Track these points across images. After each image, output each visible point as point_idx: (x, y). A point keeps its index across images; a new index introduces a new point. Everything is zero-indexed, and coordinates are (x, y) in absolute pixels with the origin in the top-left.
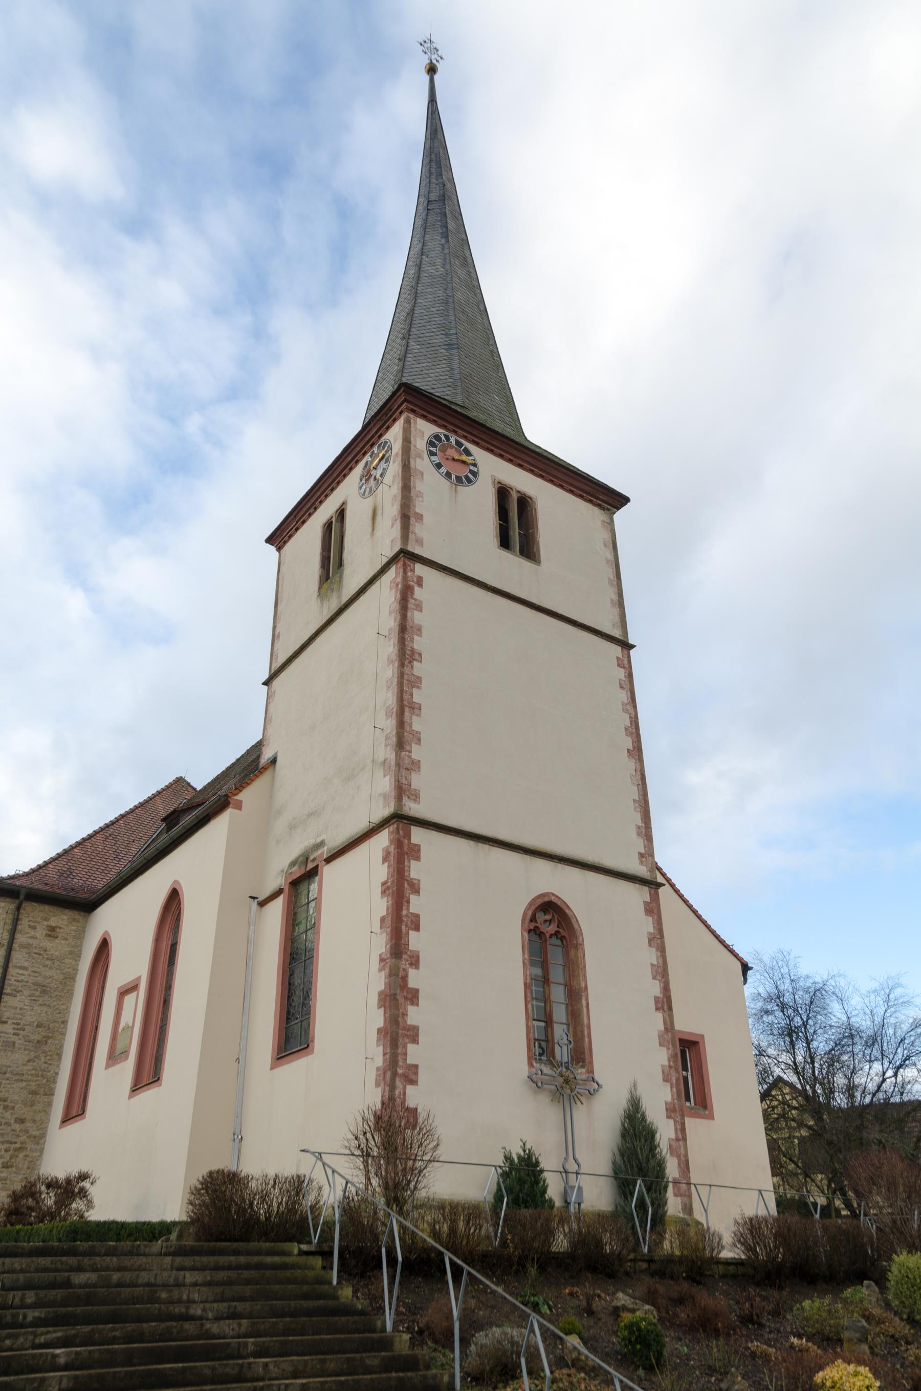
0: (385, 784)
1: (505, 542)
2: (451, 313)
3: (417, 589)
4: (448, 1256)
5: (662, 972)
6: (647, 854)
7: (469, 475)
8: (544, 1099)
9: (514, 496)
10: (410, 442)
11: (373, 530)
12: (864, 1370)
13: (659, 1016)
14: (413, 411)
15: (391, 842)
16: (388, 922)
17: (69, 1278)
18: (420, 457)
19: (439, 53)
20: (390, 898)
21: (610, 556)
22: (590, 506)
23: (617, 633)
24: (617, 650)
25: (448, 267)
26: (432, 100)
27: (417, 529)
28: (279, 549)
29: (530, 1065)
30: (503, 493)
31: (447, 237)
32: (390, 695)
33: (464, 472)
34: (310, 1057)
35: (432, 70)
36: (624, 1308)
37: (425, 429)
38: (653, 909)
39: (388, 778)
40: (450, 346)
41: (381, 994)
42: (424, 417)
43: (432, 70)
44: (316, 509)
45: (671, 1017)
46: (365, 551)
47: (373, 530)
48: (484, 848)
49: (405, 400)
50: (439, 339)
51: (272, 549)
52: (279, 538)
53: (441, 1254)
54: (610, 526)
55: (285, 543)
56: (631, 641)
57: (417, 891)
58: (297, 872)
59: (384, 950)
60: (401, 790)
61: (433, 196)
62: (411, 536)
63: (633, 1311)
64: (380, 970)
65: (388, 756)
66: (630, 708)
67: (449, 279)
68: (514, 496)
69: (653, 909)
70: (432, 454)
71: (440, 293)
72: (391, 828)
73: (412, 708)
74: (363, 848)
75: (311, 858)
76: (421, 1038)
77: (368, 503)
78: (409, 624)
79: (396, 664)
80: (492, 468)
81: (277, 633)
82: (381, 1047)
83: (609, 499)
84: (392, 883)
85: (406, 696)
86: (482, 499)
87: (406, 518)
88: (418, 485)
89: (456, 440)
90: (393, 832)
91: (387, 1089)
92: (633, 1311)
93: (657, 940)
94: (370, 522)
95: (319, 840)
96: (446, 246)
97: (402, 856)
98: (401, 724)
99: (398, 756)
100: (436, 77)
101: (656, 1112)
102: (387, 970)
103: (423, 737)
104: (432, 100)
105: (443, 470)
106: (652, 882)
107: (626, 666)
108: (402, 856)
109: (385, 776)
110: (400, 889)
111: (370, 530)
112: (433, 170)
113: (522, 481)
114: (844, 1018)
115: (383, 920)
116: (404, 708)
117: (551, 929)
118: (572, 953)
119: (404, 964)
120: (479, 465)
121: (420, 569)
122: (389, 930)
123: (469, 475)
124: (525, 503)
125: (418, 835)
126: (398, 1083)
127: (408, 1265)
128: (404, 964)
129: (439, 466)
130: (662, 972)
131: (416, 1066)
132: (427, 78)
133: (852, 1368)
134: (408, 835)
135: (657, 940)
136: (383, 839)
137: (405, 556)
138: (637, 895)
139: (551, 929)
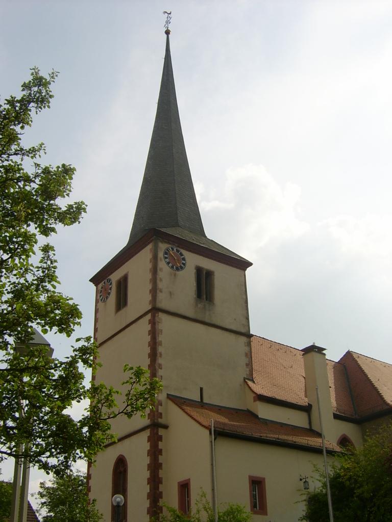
7: (182, 265)
17: (70, 167)
35: (167, 32)
39: (150, 336)
43: (167, 32)
46: (139, 299)
70: (166, 258)
74: (141, 320)
80: (193, 260)
83: (243, 264)
86: (188, 278)
87: (154, 291)
88: (161, 275)
100: (170, 36)
105: (170, 265)
108: (154, 317)
109: (149, 335)
110: (154, 333)
113: (207, 264)
114: (305, 502)
120: (186, 260)
123: (182, 265)
129: (168, 263)
132: (166, 36)
136: (149, 316)
137: (155, 310)
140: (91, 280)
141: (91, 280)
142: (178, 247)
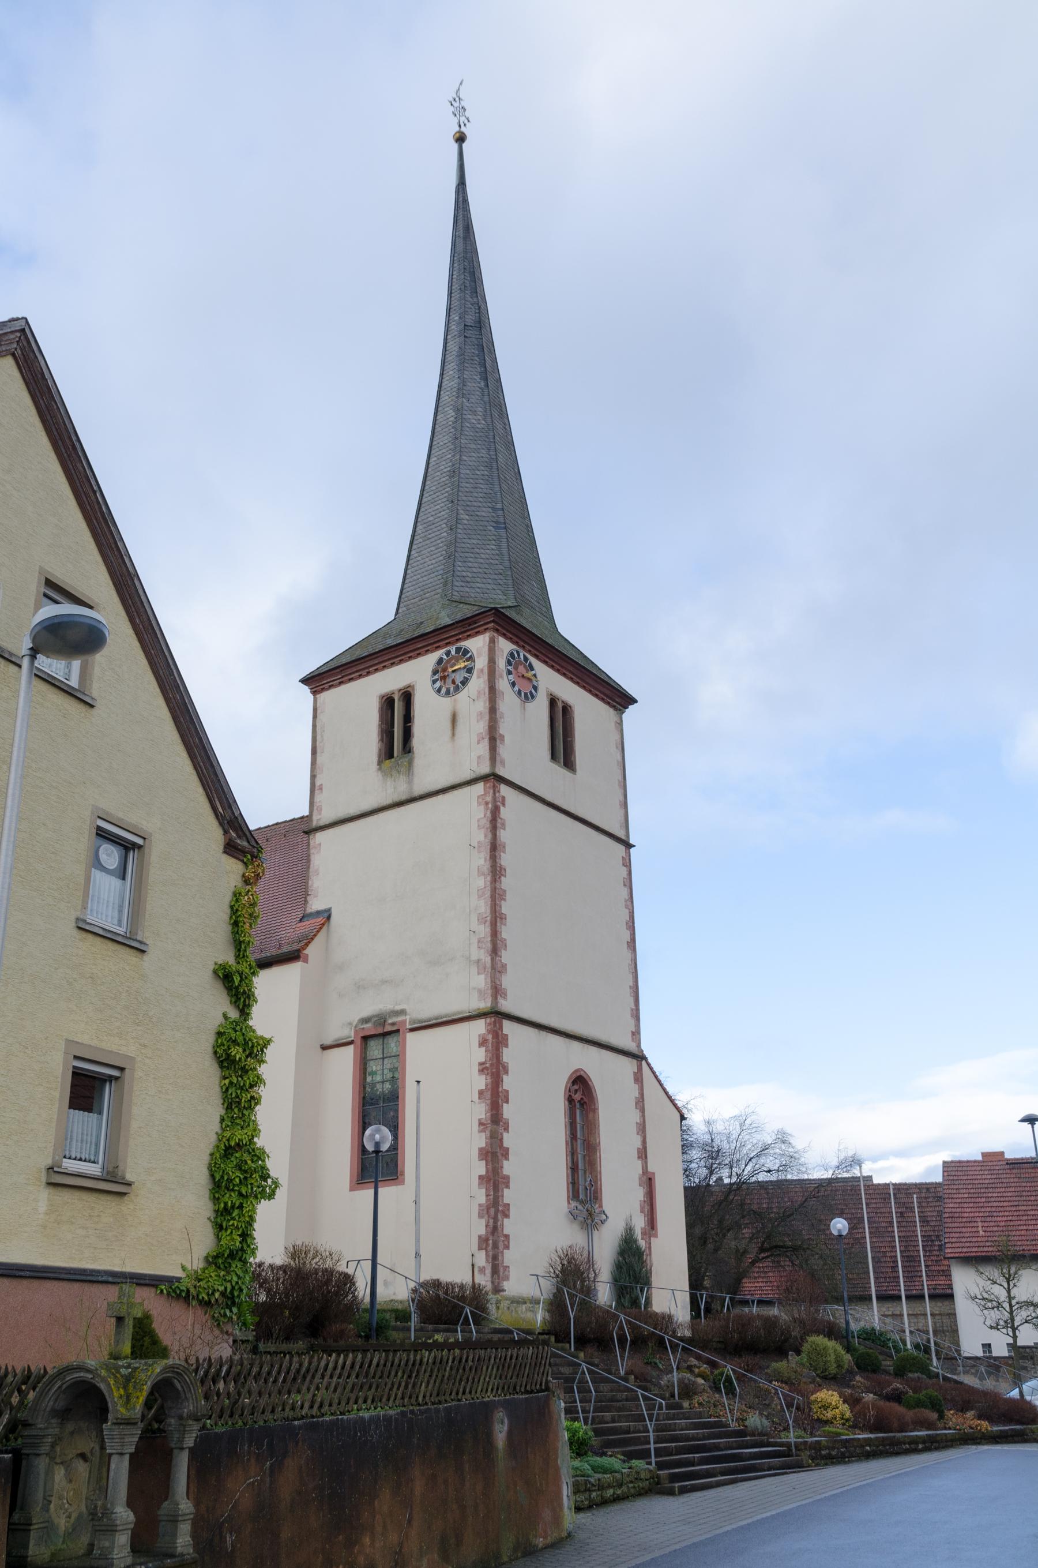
0: (481, 981)
1: (554, 757)
2: (496, 483)
3: (502, 808)
4: (666, 1337)
5: (642, 1129)
6: (636, 1034)
8: (576, 1227)
9: (560, 705)
10: (495, 663)
11: (453, 735)
12: (835, 1393)
13: (640, 1162)
14: (497, 631)
15: (489, 1031)
16: (488, 1095)
18: (501, 676)
19: (467, 113)
20: (489, 1077)
21: (620, 758)
22: (607, 707)
23: (621, 834)
24: (622, 848)
25: (489, 419)
26: (461, 184)
27: (503, 751)
28: (314, 693)
29: (569, 1203)
30: (553, 701)
31: (486, 379)
32: (482, 903)
33: (528, 688)
34: (399, 1187)
35: (461, 139)
36: (695, 1366)
37: (505, 646)
38: (638, 1078)
40: (497, 525)
41: (481, 1150)
42: (504, 636)
43: (461, 139)
44: (368, 673)
45: (646, 1163)
47: (453, 735)
48: (544, 1034)
49: (493, 621)
50: (485, 512)
51: (306, 689)
52: (318, 681)
53: (663, 1338)
54: (620, 724)
55: (323, 690)
56: (631, 842)
57: (507, 1073)
58: (369, 1028)
59: (483, 1116)
60: (497, 991)
61: (469, 322)
62: (498, 758)
63: (699, 1367)
64: (480, 1131)
65: (482, 957)
66: (629, 903)
67: (491, 437)
68: (560, 705)
69: (638, 1078)
70: (509, 673)
71: (484, 453)
72: (488, 1020)
73: (501, 918)
75: (390, 1021)
76: (511, 1185)
77: (445, 704)
78: (498, 842)
79: (489, 878)
80: (550, 680)
81: (318, 783)
82: (484, 1190)
84: (491, 1065)
85: (498, 908)
87: (494, 739)
88: (503, 707)
89: (525, 656)
90: (490, 1024)
91: (491, 1221)
92: (699, 1367)
93: (640, 1103)
94: (449, 725)
95: (398, 1008)
96: (486, 391)
97: (496, 1042)
98: (495, 933)
99: (492, 960)
100: (464, 145)
101: (638, 1234)
102: (488, 1133)
103: (508, 943)
104: (461, 184)
105: (516, 688)
106: (639, 1057)
107: (627, 863)
108: (496, 1042)
111: (449, 733)
112: (468, 283)
115: (481, 1093)
116: (496, 919)
117: (581, 1094)
118: (591, 1115)
119: (501, 1129)
121: (504, 790)
122: (489, 1102)
124: (567, 709)
125: (508, 1027)
126: (500, 1217)
127: (633, 1342)
128: (501, 1129)
130: (642, 1129)
131: (509, 1205)
132: (456, 146)
133: (830, 1392)
134: (501, 1028)
135: (640, 1103)
138: (628, 1065)
139: (581, 1094)
140: (305, 681)
141: (305, 681)
142: (529, 652)
